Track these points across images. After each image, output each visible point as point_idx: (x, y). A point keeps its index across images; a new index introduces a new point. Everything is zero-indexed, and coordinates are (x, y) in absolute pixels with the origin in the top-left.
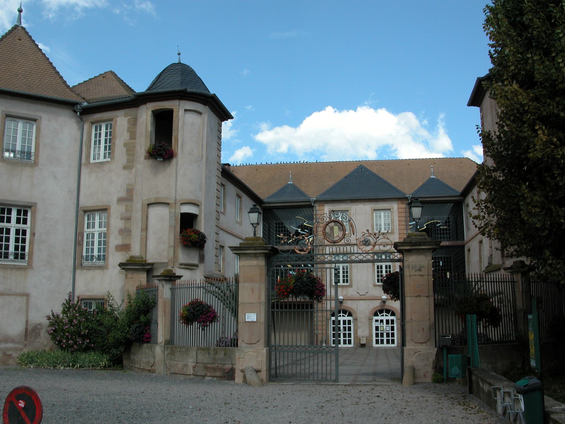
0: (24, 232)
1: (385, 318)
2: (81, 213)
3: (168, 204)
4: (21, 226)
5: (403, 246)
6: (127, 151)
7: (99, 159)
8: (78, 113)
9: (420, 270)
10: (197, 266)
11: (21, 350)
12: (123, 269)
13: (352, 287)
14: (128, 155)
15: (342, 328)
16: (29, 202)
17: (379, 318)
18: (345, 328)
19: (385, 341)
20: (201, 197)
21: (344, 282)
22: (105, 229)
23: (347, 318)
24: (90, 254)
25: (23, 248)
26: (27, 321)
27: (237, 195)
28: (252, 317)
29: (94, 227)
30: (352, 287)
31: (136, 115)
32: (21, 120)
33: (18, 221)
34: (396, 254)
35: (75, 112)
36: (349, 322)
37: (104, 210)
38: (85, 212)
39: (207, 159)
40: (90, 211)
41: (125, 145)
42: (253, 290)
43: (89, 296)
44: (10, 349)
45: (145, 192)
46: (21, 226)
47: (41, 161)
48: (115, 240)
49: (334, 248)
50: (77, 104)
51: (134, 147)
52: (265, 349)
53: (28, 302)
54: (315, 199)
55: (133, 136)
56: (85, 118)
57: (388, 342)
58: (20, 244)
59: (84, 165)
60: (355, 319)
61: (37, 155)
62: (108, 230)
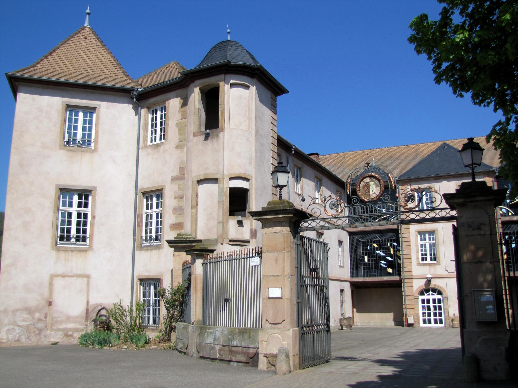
0: (86, 215)
1: (431, 298)
2: (140, 195)
4: (83, 210)
6: (179, 130)
7: (155, 141)
9: (479, 228)
10: (248, 242)
11: (83, 330)
12: (171, 247)
13: (440, 264)
14: (180, 134)
15: (432, 307)
16: (89, 187)
17: (426, 297)
18: (435, 307)
19: (433, 321)
20: (250, 171)
21: (431, 260)
23: (437, 297)
25: (85, 232)
26: (88, 302)
27: (316, 177)
28: (275, 292)
29: (152, 208)
30: (440, 264)
32: (81, 110)
33: (80, 205)
34: (448, 211)
36: (439, 301)
39: (257, 132)
41: (177, 125)
42: (276, 260)
44: (70, 330)
46: (83, 210)
47: (101, 146)
50: (133, 90)
52: (291, 330)
53: (88, 284)
54: (397, 178)
57: (436, 322)
58: (82, 227)
59: (142, 148)
60: (157, 146)
61: (96, 142)
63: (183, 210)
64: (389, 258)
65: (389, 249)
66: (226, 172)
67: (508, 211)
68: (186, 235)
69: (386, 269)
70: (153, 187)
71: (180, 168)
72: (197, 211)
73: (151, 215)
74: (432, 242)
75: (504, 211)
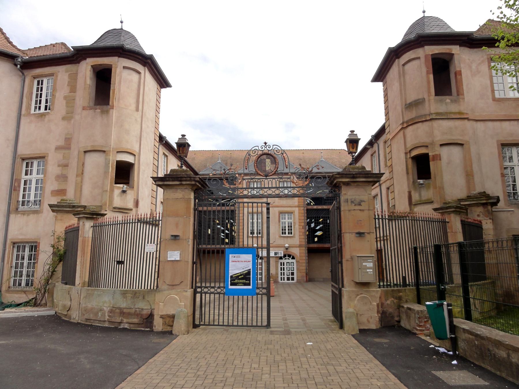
2: (18, 160)
3: (104, 151)
5: (342, 177)
8: (19, 66)
9: (360, 205)
10: (131, 210)
12: (53, 211)
14: (67, 107)
19: (286, 279)
22: (42, 176)
24: (26, 199)
31: (77, 71)
35: (16, 65)
37: (42, 158)
38: (23, 159)
40: (28, 160)
41: (65, 98)
43: (22, 239)
45: (82, 141)
48: (51, 185)
49: (266, 181)
51: (74, 99)
55: (73, 89)
56: (26, 72)
59: (24, 115)
60: (42, 115)
62: (45, 176)
63: (67, 177)
64: (227, 232)
65: (227, 224)
66: (113, 145)
67: (311, 202)
68: (70, 200)
69: (223, 239)
70: (34, 154)
71: (66, 138)
72: (82, 179)
73: (31, 181)
74: (41, 176)
75: (309, 202)
